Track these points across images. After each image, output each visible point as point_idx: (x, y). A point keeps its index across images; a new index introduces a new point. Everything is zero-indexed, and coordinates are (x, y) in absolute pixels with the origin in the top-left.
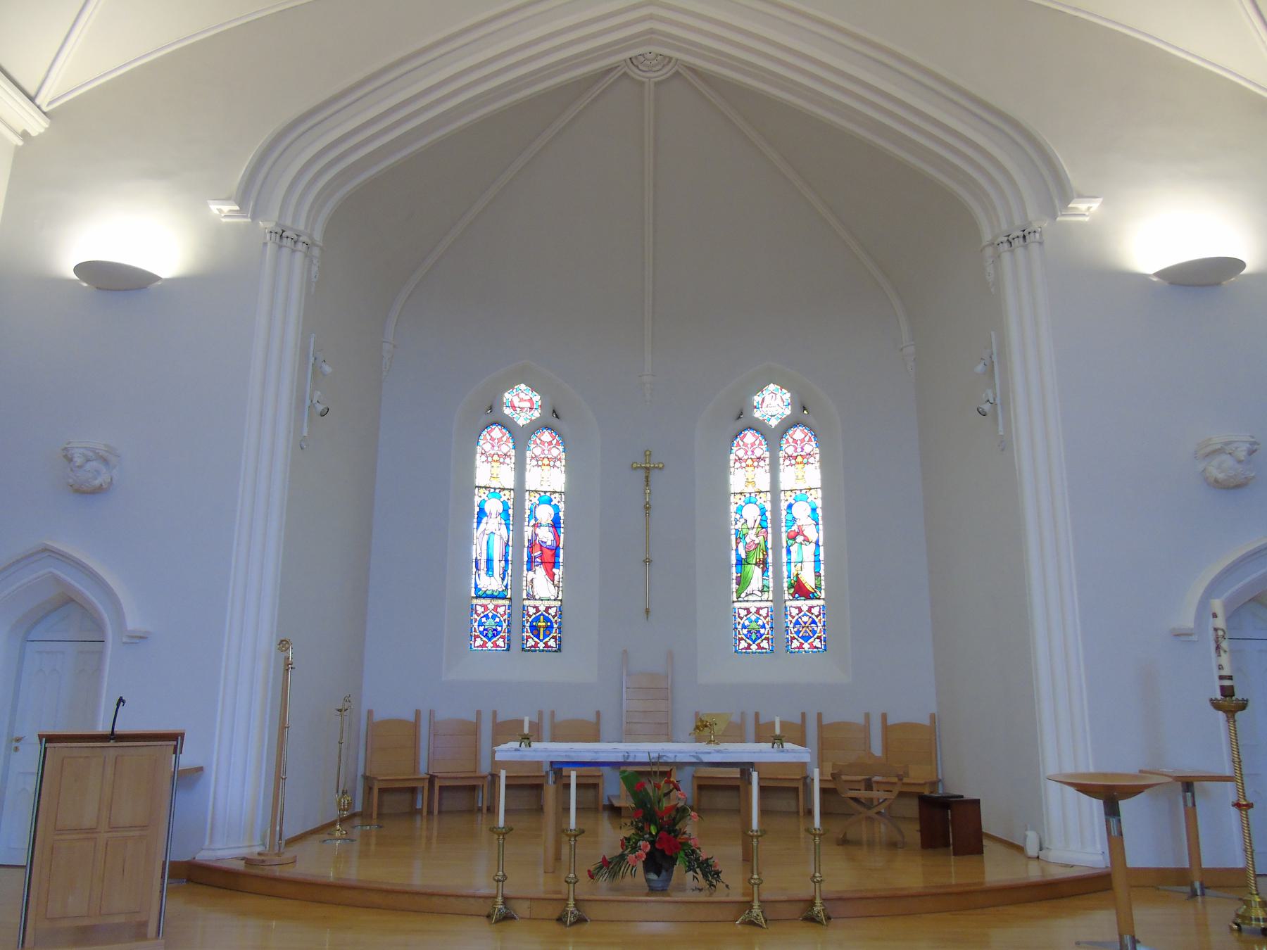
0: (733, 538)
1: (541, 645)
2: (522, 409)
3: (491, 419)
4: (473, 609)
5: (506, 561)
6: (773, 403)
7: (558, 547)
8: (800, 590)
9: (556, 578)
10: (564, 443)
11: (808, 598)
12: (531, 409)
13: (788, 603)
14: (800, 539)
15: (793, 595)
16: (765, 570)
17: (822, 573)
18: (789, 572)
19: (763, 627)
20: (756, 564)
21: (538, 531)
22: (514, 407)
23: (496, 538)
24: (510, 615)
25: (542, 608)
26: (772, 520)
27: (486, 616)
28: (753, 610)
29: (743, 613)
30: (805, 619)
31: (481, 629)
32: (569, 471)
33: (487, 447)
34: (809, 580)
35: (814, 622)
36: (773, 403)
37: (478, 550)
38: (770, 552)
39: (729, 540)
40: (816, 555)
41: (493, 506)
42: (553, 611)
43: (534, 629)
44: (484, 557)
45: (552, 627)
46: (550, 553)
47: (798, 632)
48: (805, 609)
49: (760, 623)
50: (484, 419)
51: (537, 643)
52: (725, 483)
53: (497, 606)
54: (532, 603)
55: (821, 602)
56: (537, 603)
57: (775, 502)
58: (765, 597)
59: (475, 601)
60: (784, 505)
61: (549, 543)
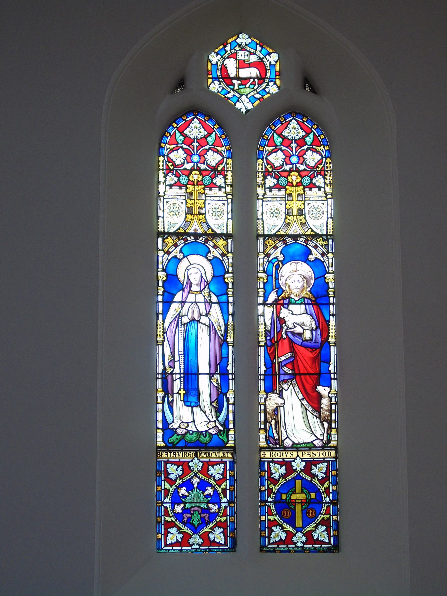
1: (300, 539)
2: (244, 81)
3: (181, 98)
4: (161, 472)
5: (224, 374)
7: (325, 341)
9: (325, 403)
10: (328, 141)
12: (262, 79)
21: (284, 313)
22: (226, 79)
23: (204, 332)
24: (234, 480)
25: (298, 465)
27: (189, 485)
31: (178, 509)
32: (342, 196)
33: (178, 157)
37: (168, 354)
41: (195, 268)
42: (319, 471)
43: (285, 508)
44: (179, 368)
45: (319, 501)
46: (308, 354)
50: (169, 103)
51: (290, 535)
53: (207, 464)
54: (278, 455)
56: (289, 455)
59: (164, 456)
61: (308, 335)
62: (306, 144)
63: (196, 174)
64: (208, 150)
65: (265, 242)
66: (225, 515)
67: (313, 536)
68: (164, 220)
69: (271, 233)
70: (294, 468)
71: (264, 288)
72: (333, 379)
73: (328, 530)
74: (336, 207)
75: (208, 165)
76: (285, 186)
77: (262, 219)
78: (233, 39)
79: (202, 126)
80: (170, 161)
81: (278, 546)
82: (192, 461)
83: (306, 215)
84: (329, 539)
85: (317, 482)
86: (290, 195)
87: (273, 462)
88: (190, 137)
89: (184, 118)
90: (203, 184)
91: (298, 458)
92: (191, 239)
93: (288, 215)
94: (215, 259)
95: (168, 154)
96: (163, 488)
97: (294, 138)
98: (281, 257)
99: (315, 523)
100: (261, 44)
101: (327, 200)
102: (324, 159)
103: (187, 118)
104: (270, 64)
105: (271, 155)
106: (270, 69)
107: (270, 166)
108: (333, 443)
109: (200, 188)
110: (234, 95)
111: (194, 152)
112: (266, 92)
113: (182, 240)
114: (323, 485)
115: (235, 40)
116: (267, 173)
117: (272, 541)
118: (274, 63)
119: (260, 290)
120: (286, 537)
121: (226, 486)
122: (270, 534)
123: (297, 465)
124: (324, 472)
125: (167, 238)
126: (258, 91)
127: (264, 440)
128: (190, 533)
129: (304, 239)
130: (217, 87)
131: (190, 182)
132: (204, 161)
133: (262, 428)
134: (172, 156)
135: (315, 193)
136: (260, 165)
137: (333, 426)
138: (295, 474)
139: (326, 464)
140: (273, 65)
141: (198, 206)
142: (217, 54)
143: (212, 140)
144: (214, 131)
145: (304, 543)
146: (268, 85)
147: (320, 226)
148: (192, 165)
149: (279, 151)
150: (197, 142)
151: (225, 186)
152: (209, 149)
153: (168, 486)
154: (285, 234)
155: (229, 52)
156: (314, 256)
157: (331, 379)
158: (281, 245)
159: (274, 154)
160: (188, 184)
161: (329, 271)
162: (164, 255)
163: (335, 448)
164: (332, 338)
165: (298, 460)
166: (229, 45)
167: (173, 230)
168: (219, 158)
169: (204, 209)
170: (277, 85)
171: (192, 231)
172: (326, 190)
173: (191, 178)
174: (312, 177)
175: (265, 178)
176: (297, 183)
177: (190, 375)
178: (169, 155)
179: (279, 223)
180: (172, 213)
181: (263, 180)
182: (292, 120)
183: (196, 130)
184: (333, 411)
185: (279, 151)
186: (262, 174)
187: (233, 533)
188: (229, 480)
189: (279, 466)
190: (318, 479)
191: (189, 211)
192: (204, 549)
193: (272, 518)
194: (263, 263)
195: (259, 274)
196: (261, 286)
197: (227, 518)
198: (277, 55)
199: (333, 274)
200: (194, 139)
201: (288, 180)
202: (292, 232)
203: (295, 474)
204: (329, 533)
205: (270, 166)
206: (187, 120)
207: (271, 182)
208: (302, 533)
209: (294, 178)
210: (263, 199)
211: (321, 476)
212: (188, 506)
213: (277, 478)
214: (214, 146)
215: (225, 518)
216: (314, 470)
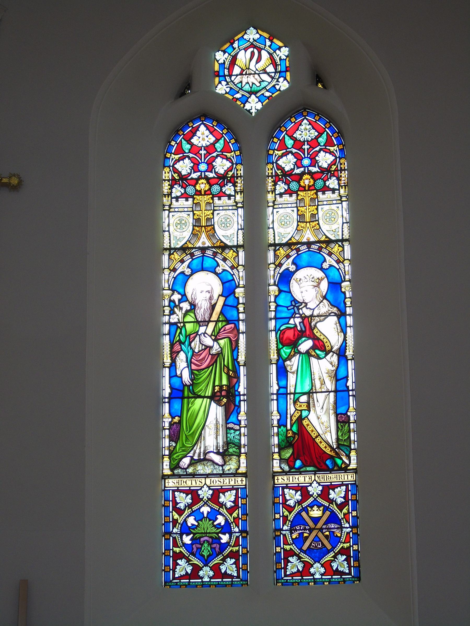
0: (166, 340)
6: (253, 68)
8: (304, 450)
11: (321, 467)
13: (280, 480)
14: (305, 345)
15: (290, 462)
16: (230, 410)
17: (352, 415)
18: (283, 414)
19: (226, 528)
20: (213, 397)
26: (253, 302)
28: (205, 493)
29: (183, 500)
30: (316, 513)
34: (322, 423)
35: (333, 518)
36: (253, 68)
38: (242, 371)
39: (159, 347)
40: (338, 378)
42: (337, 495)
47: (300, 540)
48: (315, 490)
49: (221, 520)
52: (154, 229)
55: (349, 477)
57: (255, 267)
58: (231, 466)
60: (272, 274)
62: (319, 145)
63: (307, 179)
64: (319, 151)
65: (276, 252)
66: (237, 544)
67: (220, 570)
68: (274, 231)
69: (282, 242)
70: (201, 497)
71: (275, 302)
72: (351, 396)
73: (348, 560)
74: (352, 210)
75: (216, 173)
76: (297, 191)
77: (169, 231)
78: (240, 36)
79: (312, 127)
80: (176, 171)
81: (292, 577)
82: (311, 485)
83: (215, 225)
84: (237, 573)
85: (225, 511)
86: (198, 204)
87: (178, 490)
88: (300, 140)
89: (191, 124)
90: (315, 189)
91: (205, 486)
92: (304, 248)
93: (300, 222)
94: (224, 272)
95: (277, 160)
96: (281, 515)
97: (306, 140)
98: (326, 266)
99: (334, 552)
100: (271, 38)
101: (341, 203)
102: (338, 159)
103: (194, 124)
104: (280, 59)
105: (178, 163)
106: (280, 65)
107: (177, 175)
108: (243, 469)
109: (207, 198)
110: (243, 95)
111: (201, 160)
112: (277, 89)
113: (295, 251)
114: (231, 515)
115: (242, 37)
116: (173, 182)
117: (288, 573)
118: (285, 58)
119: (165, 308)
120: (192, 570)
121: (238, 515)
122: (286, 565)
123: (314, 490)
124: (342, 496)
125: (279, 249)
126: (267, 89)
127: (168, 467)
128: (201, 564)
129: (317, 247)
130: (225, 87)
131: (301, 188)
132: (212, 170)
133: (275, 452)
134: (177, 166)
135: (329, 196)
136: (270, 169)
137: (243, 450)
138: (311, 499)
139: (235, 491)
140: (283, 59)
141: (206, 217)
142: (224, 52)
143: (323, 140)
144: (223, 136)
145: (211, 578)
146: (278, 81)
147: (229, 236)
148: (199, 174)
149: (187, 159)
150: (308, 144)
151: (235, 194)
152: (218, 156)
153: (176, 516)
154: (192, 246)
155: (237, 48)
156: (328, 263)
157: (349, 396)
158: (188, 260)
159: (181, 162)
160: (299, 190)
161: (239, 284)
162: (170, 273)
163: (244, 475)
164: (241, 358)
165: (315, 484)
166: (237, 42)
167: (284, 241)
168: (228, 164)
169: (212, 220)
170: (287, 81)
171: (305, 240)
172: (341, 193)
173: (302, 184)
174: (325, 179)
175: (172, 187)
176: (205, 191)
177: (186, 400)
178: (175, 166)
179: (187, 234)
180: (177, 227)
181: (273, 185)
182: (303, 120)
183: (203, 137)
184: (242, 435)
185: (187, 159)
186: (169, 183)
187: (246, 566)
188: (241, 507)
189: (294, 492)
190: (226, 508)
191: (301, 218)
192: (193, 582)
193: (288, 547)
194: (274, 275)
195: (270, 287)
196: (273, 299)
197: (239, 548)
198: (287, 49)
199: (243, 289)
200: (304, 141)
201: (195, 189)
202: (199, 244)
203: (311, 499)
204: (349, 563)
205: (177, 175)
206: (194, 126)
207: (281, 187)
208: (320, 564)
209: (202, 186)
210: (273, 206)
211: (340, 501)
212: (198, 536)
213: (182, 508)
214: (223, 152)
215: (237, 548)
216: (332, 495)
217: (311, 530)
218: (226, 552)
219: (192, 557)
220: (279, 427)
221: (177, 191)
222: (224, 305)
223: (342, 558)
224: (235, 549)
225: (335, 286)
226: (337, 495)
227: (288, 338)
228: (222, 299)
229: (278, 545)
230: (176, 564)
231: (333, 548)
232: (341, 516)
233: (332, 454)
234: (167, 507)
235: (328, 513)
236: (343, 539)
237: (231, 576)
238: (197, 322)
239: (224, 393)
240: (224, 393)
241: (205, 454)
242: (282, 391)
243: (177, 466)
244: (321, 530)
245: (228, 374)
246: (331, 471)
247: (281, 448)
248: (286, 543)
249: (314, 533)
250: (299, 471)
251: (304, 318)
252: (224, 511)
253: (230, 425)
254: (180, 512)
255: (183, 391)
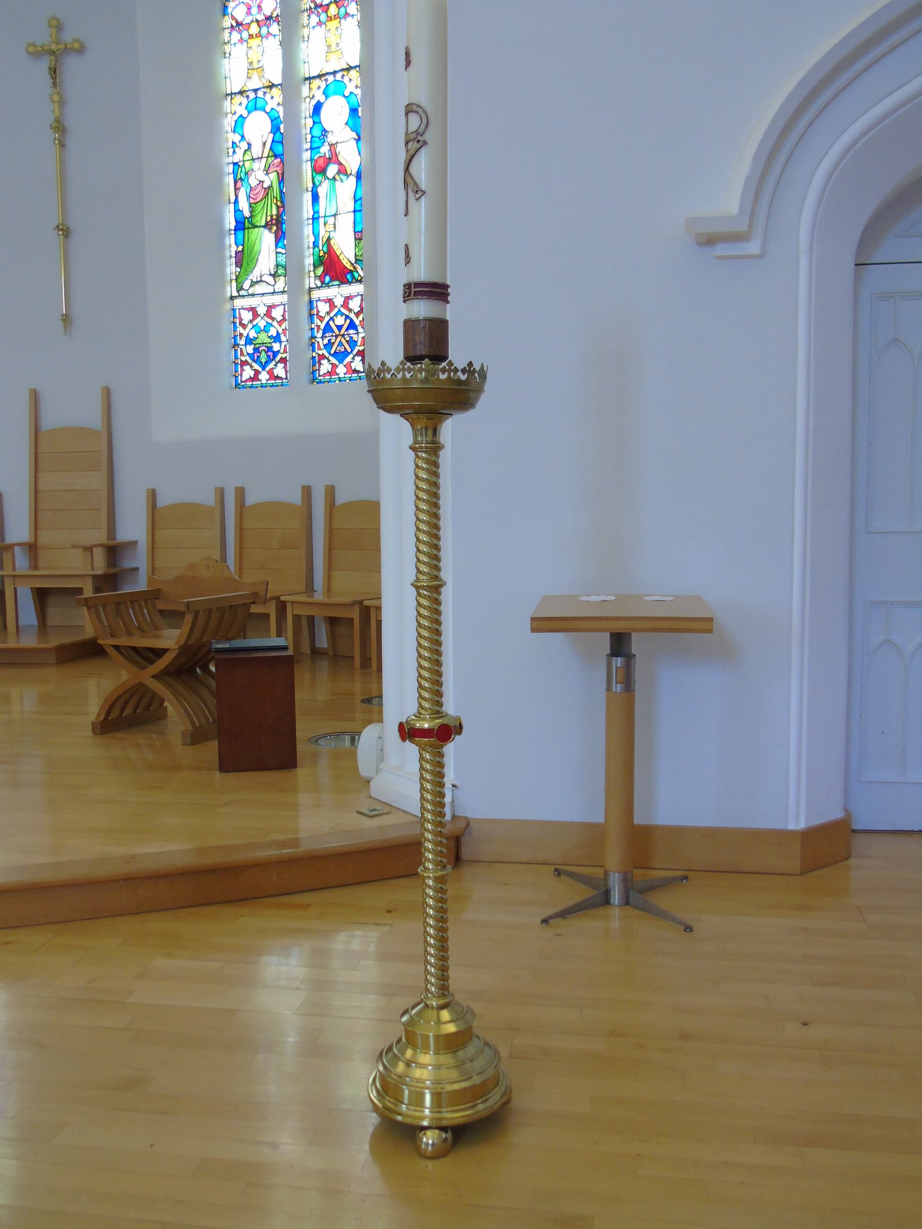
8: (332, 269)
11: (344, 281)
14: (332, 170)
15: (321, 278)
18: (316, 235)
28: (262, 310)
29: (247, 316)
30: (340, 320)
35: (352, 325)
42: (355, 304)
47: (329, 345)
48: (339, 301)
49: (273, 332)
51: (257, 373)
66: (285, 352)
114: (357, 317)
128: (260, 369)
217: (336, 336)
218: (278, 359)
219: (254, 364)
220: (314, 248)
221: (235, 36)
222: (273, 141)
223: (358, 359)
224: (284, 356)
225: (354, 111)
226: (355, 304)
227: (320, 166)
228: (271, 136)
229: (313, 350)
230: (242, 370)
231: (352, 351)
232: (357, 323)
233: (352, 268)
234: (234, 323)
235: (348, 321)
236: (359, 343)
237: (281, 378)
238: (253, 159)
239: (274, 222)
240: (274, 222)
241: (261, 276)
242: (316, 215)
243: (242, 288)
244: (343, 336)
245: (276, 204)
246: (349, 283)
247: (315, 267)
248: (319, 349)
249: (339, 338)
250: (328, 286)
251: (331, 145)
252: (275, 323)
253: (279, 250)
254: (244, 326)
255: (244, 223)
